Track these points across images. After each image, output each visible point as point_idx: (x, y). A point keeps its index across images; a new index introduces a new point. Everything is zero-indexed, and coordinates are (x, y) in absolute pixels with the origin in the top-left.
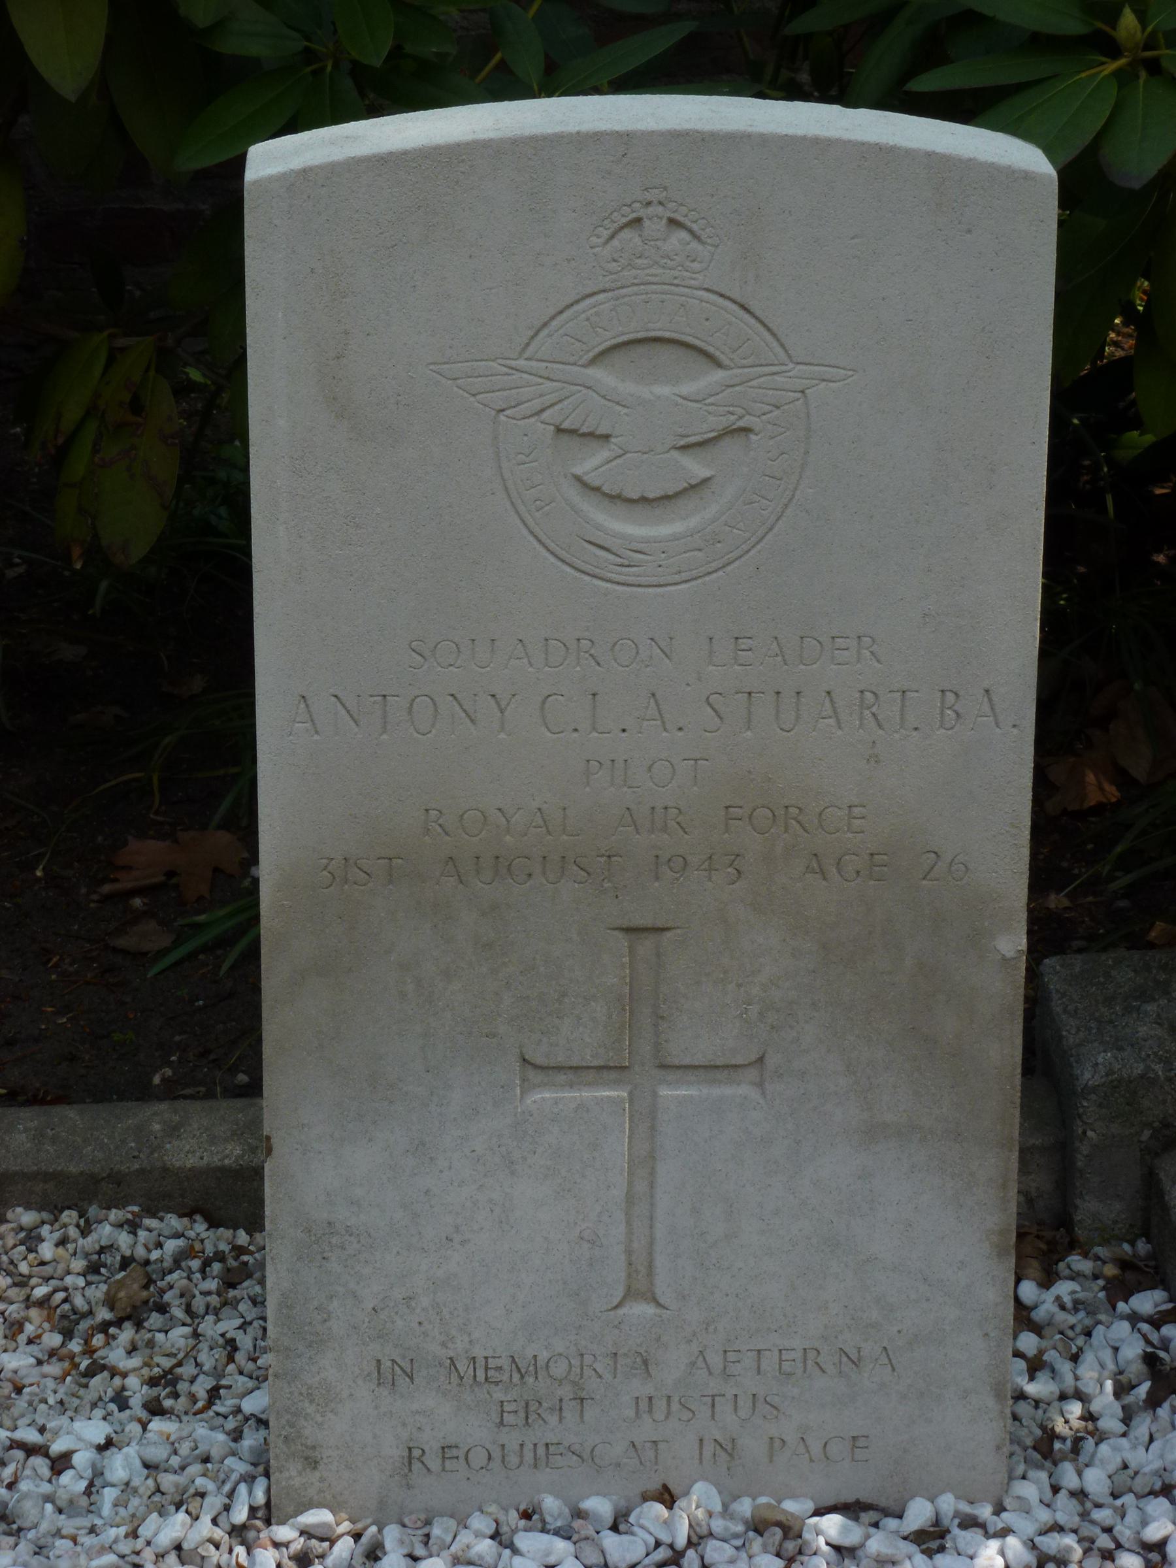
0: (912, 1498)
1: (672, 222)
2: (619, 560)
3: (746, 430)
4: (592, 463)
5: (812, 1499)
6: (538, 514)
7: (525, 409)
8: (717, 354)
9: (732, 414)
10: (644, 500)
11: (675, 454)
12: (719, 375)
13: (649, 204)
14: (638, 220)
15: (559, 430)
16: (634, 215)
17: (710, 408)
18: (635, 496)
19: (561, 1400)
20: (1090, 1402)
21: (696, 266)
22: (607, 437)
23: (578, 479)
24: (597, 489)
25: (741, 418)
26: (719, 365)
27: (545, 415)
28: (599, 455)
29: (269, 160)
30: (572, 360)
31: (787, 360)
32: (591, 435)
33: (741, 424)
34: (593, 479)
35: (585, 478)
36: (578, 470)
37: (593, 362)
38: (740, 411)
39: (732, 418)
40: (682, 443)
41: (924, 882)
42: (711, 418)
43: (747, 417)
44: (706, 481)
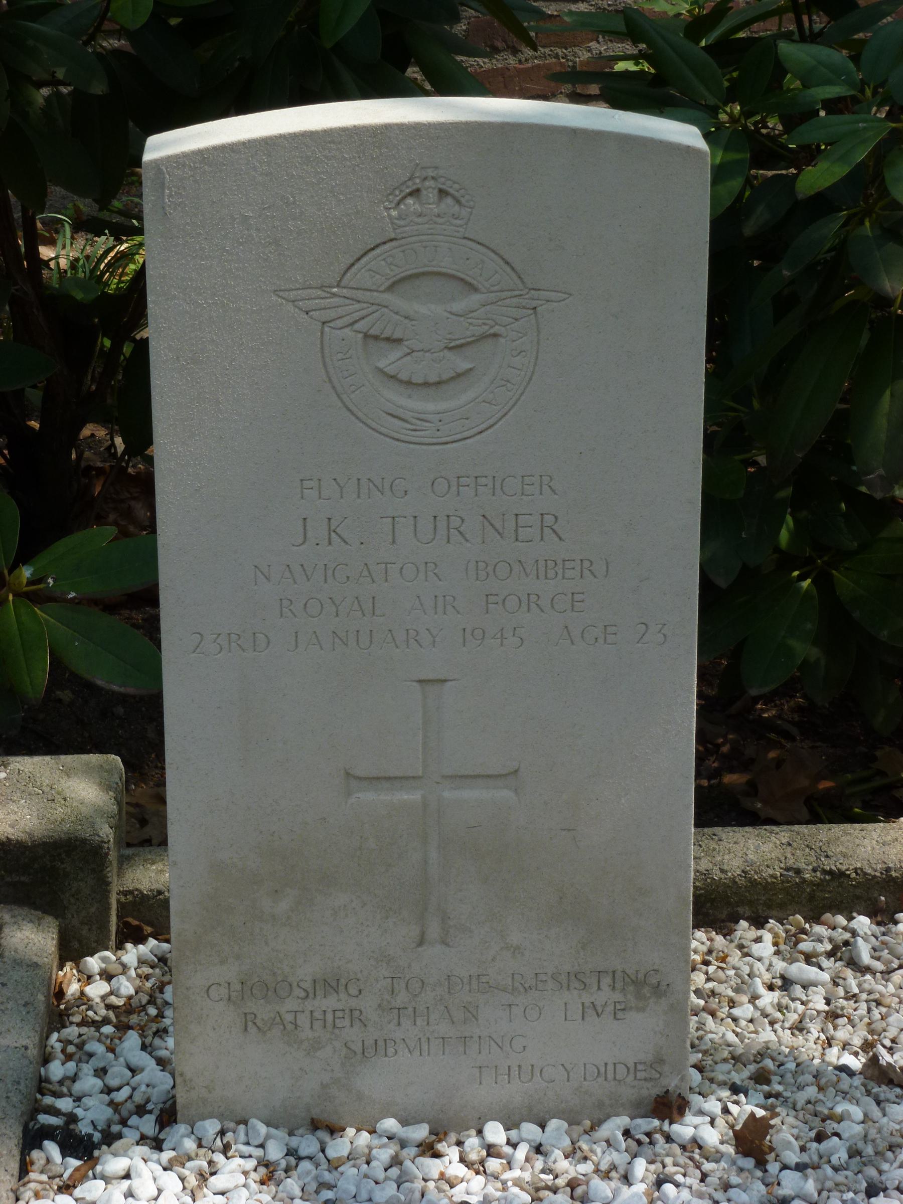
0: (484, 1124)
1: (441, 191)
2: (409, 426)
3: (495, 335)
4: (390, 359)
5: (428, 1123)
6: (352, 396)
7: (339, 323)
8: (475, 282)
9: (484, 324)
10: (426, 384)
11: (446, 351)
12: (476, 298)
13: (425, 179)
14: (418, 191)
15: (366, 336)
16: (414, 187)
17: (469, 320)
18: (420, 381)
19: (352, 1026)
20: (296, 1151)
21: (458, 222)
22: (399, 341)
23: (381, 371)
24: (393, 377)
25: (492, 327)
26: (476, 290)
27: (357, 326)
28: (395, 354)
29: (164, 146)
30: (374, 287)
31: (521, 286)
32: (388, 339)
33: (492, 331)
34: (390, 370)
35: (385, 370)
36: (381, 365)
37: (391, 288)
38: (493, 323)
39: (487, 327)
40: (452, 344)
41: (639, 645)
42: (471, 328)
43: (497, 327)
44: (471, 369)
